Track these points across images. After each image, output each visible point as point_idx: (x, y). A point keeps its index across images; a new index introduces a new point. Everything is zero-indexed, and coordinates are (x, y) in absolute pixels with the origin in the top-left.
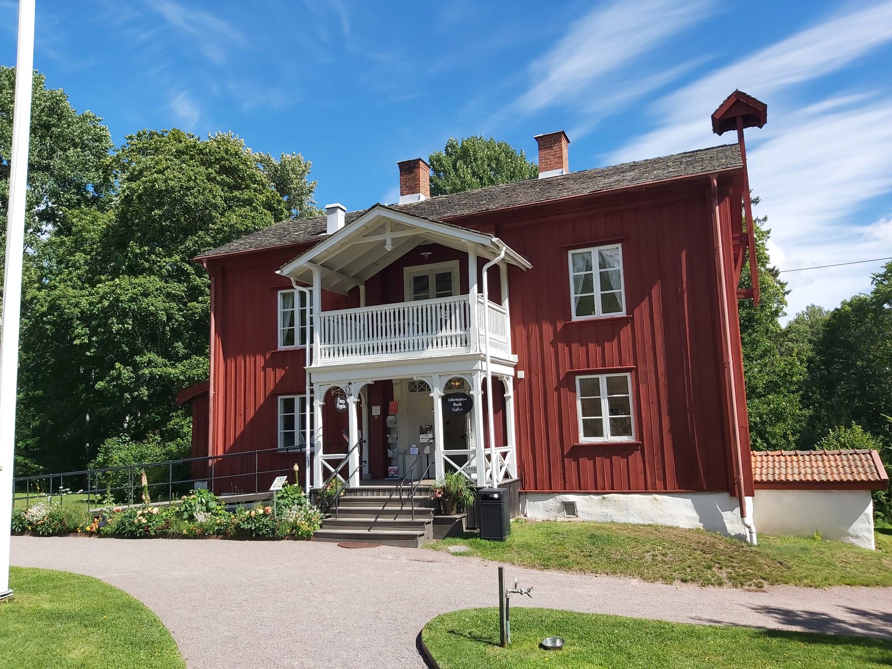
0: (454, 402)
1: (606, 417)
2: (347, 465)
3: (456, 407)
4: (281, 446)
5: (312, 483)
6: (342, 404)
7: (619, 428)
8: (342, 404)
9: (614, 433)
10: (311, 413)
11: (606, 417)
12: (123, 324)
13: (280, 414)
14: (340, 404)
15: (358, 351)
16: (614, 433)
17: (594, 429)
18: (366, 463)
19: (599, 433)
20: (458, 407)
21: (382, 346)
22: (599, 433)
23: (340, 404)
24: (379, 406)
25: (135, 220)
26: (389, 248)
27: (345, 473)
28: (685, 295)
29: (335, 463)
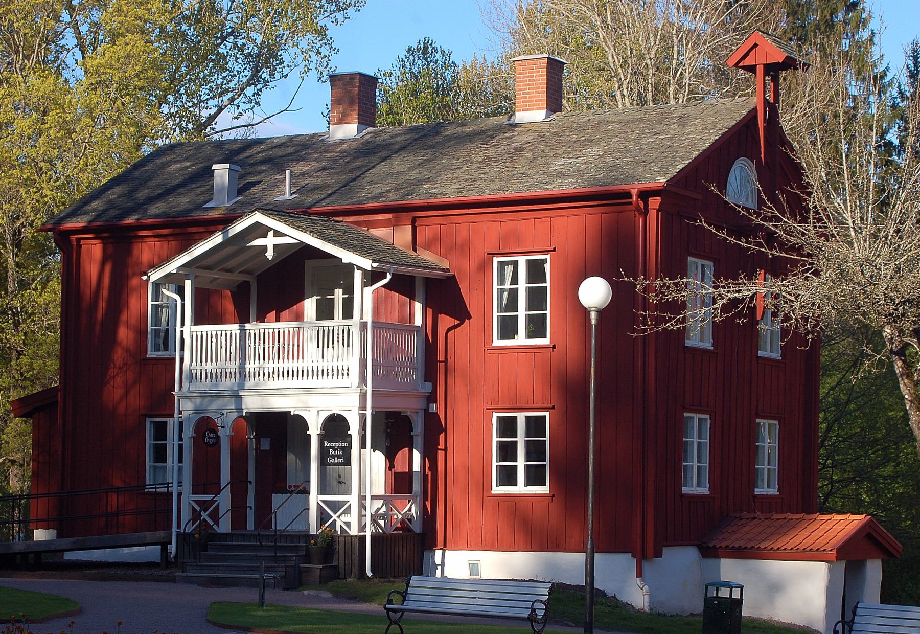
0: (331, 448)
1: (521, 463)
2: (218, 507)
3: (333, 456)
4: (150, 482)
5: (179, 527)
6: (212, 438)
7: (534, 477)
8: (212, 438)
9: (530, 482)
10: (180, 442)
11: (521, 463)
12: (901, 376)
13: (149, 441)
14: (209, 438)
15: (330, 371)
16: (530, 482)
17: (508, 477)
18: (251, 509)
19: (514, 483)
20: (336, 456)
21: (298, 371)
22: (514, 483)
23: (209, 438)
24: (269, 439)
25: (860, 413)
26: (270, 254)
27: (215, 516)
28: (217, 239)
29: (204, 505)
